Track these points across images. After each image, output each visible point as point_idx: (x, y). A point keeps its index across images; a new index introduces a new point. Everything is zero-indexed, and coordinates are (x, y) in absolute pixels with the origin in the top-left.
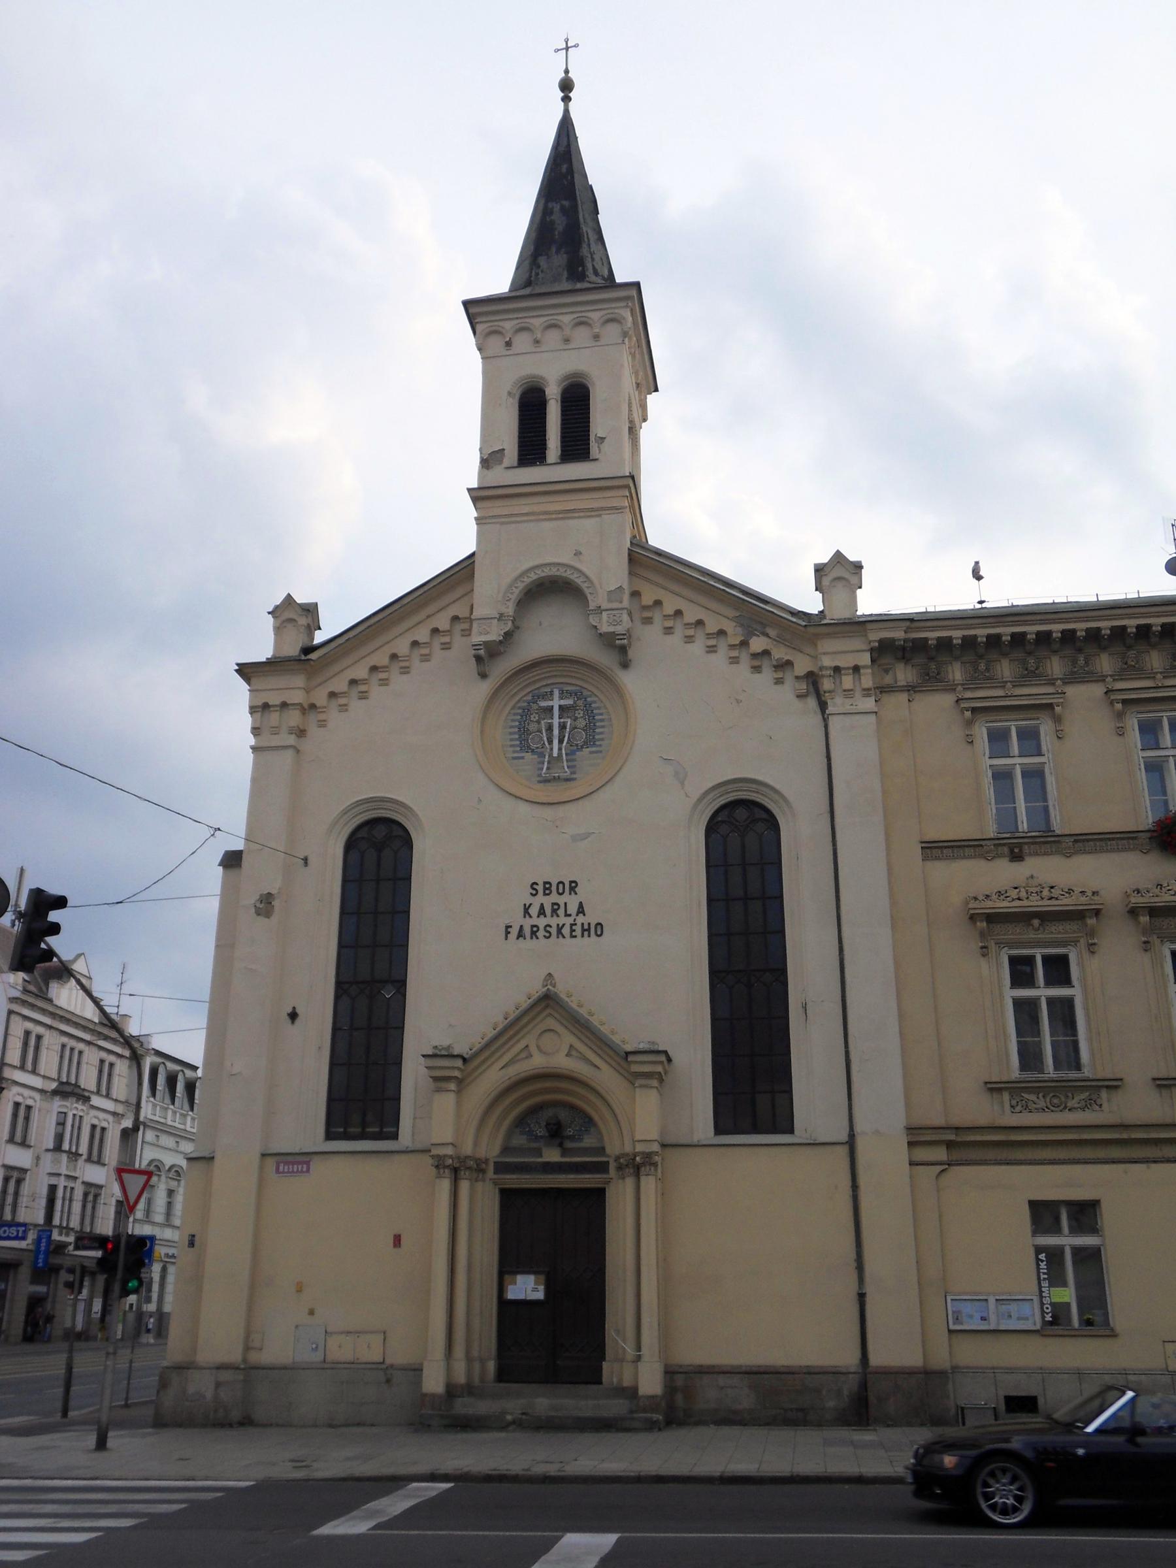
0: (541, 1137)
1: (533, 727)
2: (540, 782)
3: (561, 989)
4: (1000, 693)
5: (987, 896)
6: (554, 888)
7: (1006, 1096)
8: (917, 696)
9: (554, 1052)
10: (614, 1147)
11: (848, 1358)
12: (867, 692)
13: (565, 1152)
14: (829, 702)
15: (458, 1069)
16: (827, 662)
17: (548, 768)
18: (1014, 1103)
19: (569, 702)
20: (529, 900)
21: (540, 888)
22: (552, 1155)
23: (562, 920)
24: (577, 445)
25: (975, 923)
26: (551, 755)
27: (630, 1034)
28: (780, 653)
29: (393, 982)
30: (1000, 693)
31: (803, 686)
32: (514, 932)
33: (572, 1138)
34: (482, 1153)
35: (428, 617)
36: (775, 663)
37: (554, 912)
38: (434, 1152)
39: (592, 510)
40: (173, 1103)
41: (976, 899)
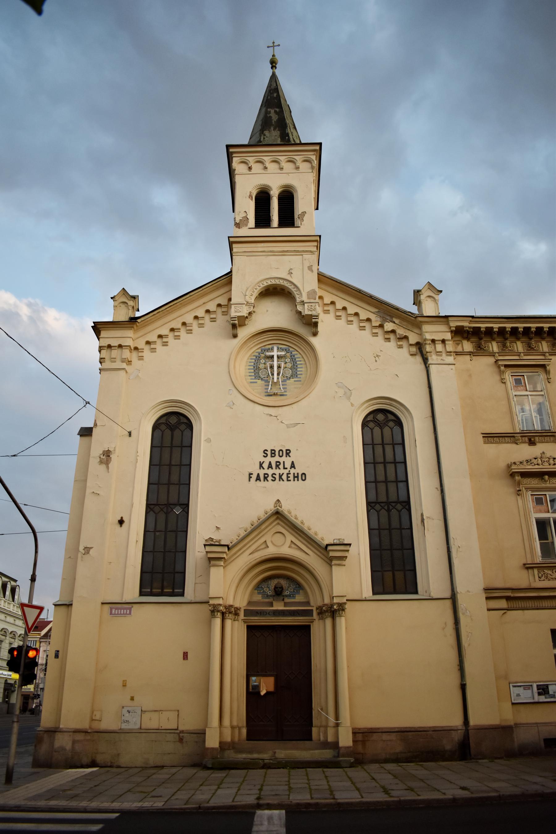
0: (271, 596)
1: (262, 366)
2: (266, 396)
3: (285, 508)
4: (517, 358)
5: (521, 463)
6: (277, 453)
7: (536, 571)
8: (474, 358)
9: (282, 545)
10: (316, 602)
11: (457, 721)
12: (449, 353)
13: (286, 604)
14: (429, 358)
15: (225, 552)
16: (428, 336)
17: (271, 389)
18: (540, 575)
19: (283, 353)
20: (262, 459)
21: (269, 453)
22: (279, 606)
23: (282, 471)
24: (288, 218)
25: (255, 589)
26: (273, 382)
27: (326, 536)
28: (401, 331)
29: (180, 505)
30: (517, 358)
31: (414, 350)
32: (254, 477)
33: (289, 596)
34: (237, 605)
35: (204, 303)
36: (398, 336)
37: (277, 466)
38: (212, 602)
39: (298, 251)
40: (4, 597)
41: (515, 463)
